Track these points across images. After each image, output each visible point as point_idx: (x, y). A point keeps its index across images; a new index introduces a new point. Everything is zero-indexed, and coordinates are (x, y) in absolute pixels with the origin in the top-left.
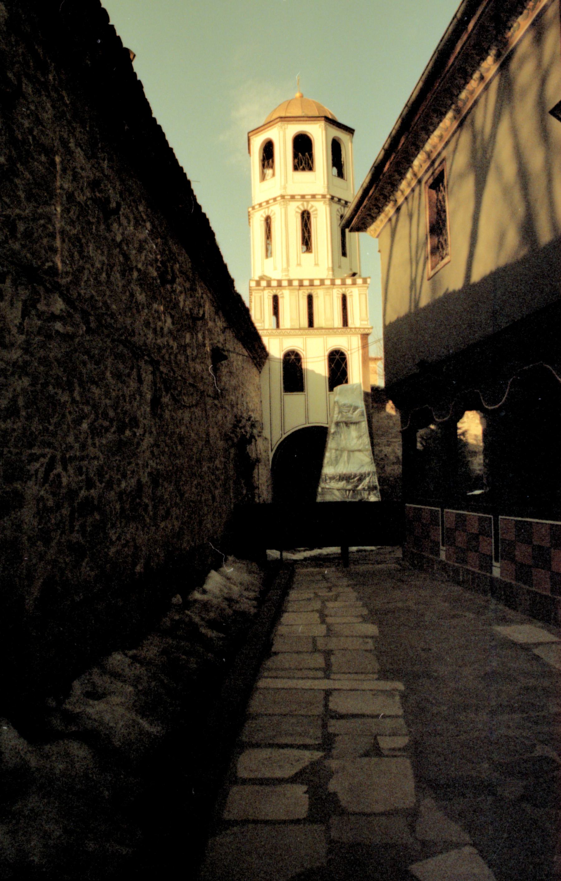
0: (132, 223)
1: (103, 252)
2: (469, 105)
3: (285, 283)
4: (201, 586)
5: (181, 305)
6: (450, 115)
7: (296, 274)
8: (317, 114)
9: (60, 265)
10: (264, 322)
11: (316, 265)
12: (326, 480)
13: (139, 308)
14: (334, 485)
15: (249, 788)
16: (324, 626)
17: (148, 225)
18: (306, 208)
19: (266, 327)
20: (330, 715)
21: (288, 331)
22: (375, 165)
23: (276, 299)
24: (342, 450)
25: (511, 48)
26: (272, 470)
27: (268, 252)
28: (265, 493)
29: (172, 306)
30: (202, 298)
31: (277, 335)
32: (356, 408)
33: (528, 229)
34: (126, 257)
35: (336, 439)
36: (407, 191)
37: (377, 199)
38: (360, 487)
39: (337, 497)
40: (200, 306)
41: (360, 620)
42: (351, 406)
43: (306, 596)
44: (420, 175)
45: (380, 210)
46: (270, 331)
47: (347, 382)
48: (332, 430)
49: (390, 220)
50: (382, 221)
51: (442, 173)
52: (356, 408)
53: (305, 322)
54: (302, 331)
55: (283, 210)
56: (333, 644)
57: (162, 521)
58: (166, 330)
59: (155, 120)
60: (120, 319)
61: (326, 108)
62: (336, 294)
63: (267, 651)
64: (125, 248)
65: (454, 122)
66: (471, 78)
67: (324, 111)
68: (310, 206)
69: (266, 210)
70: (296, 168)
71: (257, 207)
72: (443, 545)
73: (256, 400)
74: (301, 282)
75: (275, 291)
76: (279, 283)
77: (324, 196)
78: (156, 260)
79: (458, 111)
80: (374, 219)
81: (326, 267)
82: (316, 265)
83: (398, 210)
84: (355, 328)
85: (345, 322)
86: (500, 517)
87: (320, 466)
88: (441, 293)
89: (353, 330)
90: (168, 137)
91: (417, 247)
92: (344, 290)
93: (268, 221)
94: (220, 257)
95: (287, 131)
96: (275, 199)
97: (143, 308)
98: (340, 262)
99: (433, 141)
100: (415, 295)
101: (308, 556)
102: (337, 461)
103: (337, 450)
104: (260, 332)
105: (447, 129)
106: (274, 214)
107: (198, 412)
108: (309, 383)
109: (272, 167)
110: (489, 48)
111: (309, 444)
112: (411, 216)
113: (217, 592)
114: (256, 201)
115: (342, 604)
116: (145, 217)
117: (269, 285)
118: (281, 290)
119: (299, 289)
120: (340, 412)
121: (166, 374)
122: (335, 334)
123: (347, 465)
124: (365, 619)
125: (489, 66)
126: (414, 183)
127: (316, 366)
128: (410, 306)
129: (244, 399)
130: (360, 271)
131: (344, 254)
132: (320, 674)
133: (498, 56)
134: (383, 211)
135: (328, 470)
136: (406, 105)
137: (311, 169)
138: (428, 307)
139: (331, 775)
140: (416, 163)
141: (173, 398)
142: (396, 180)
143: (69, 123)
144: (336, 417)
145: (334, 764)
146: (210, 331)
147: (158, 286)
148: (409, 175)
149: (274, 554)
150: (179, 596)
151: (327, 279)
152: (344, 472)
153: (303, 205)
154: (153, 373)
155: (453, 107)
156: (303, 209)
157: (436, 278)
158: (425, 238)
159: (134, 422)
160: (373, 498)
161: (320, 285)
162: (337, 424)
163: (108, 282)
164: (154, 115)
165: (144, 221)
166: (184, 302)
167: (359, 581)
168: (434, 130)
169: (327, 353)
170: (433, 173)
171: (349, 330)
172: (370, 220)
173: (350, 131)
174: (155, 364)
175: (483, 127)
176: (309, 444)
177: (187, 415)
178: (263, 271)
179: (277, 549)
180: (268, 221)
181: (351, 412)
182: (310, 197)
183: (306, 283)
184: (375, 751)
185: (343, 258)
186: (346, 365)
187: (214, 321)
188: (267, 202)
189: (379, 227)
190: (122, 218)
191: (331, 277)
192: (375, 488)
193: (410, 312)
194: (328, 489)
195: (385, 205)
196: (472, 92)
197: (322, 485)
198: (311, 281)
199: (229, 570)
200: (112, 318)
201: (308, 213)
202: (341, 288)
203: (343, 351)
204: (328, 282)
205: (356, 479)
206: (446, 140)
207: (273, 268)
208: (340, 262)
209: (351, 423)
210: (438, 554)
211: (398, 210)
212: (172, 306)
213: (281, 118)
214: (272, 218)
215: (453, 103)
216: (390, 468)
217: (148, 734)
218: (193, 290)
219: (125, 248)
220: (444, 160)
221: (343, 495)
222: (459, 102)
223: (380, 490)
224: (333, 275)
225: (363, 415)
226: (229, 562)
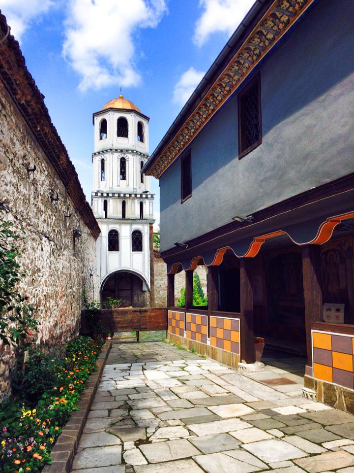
1: (26, 189)
7: (116, 189)
17: (46, 173)
30: (69, 205)
60: (33, 220)
68: (125, 156)
86: (312, 331)
109: (106, 133)
116: (45, 169)
131: (142, 181)
143: (14, 130)
173: (147, 118)
178: (99, 187)
183: (122, 195)
200: (29, 220)
210: (183, 336)
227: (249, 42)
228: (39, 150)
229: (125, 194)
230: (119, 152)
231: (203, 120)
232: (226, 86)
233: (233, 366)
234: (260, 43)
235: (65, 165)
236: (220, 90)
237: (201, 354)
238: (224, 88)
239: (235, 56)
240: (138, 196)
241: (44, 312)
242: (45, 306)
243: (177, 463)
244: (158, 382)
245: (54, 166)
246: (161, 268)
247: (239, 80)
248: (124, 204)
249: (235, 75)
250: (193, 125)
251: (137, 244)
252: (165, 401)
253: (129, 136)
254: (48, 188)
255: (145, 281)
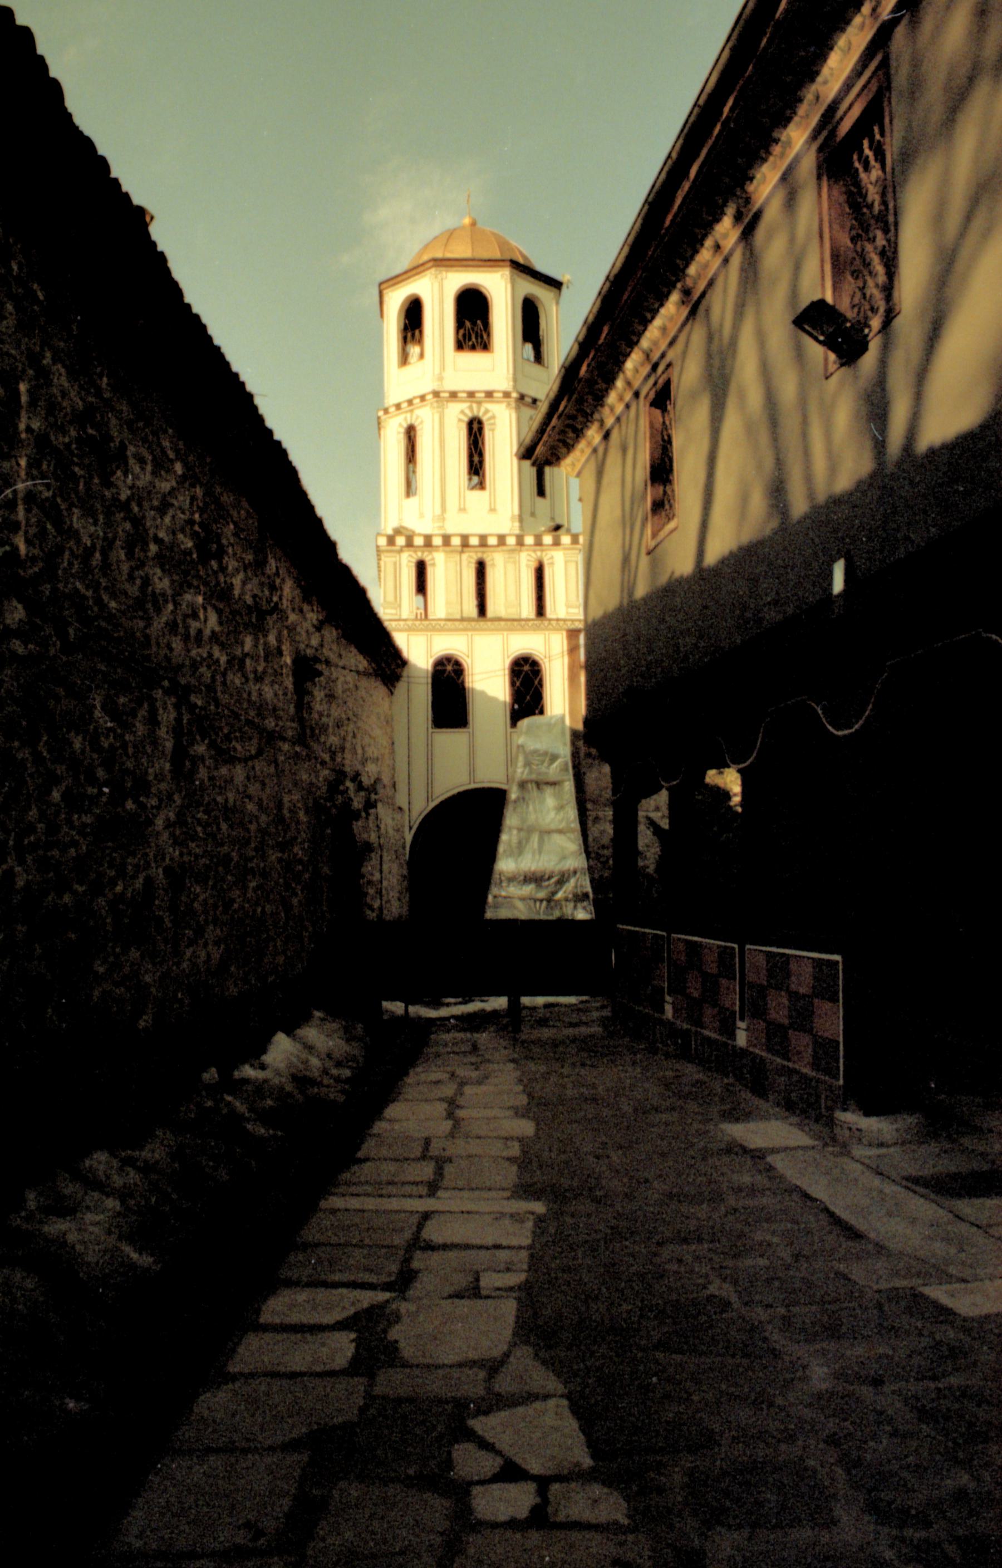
0: (149, 468)
2: (701, 286)
3: (437, 541)
4: (258, 1057)
5: (237, 592)
6: (675, 297)
7: (456, 525)
8: (498, 255)
9: (22, 548)
10: (400, 606)
11: (493, 510)
12: (501, 881)
13: (158, 601)
14: (514, 890)
15: (268, 1336)
16: (450, 1123)
17: (178, 468)
18: (476, 413)
19: (404, 616)
20: (418, 1244)
21: (442, 623)
22: (567, 364)
23: (421, 568)
24: (530, 830)
25: (755, 210)
26: (410, 864)
27: (410, 488)
28: (395, 903)
29: (220, 596)
30: (277, 574)
31: (421, 630)
32: (554, 758)
33: (778, 492)
34: (137, 522)
35: (519, 810)
36: (620, 408)
37: (573, 417)
38: (560, 895)
39: (521, 911)
40: (273, 588)
41: (511, 1113)
42: (546, 753)
43: (433, 1077)
44: (636, 384)
45: (579, 434)
46: (410, 623)
47: (542, 712)
48: (513, 795)
49: (595, 451)
50: (582, 451)
51: (668, 383)
52: (554, 758)
53: (471, 607)
54: (465, 623)
55: (437, 417)
56: (458, 1148)
57: (187, 947)
58: (207, 632)
59: (188, 306)
61: (514, 243)
62: (526, 563)
63: (349, 1158)
64: (136, 509)
65: (683, 307)
66: (702, 245)
67: (511, 249)
68: (482, 410)
69: (408, 415)
70: (460, 346)
71: (392, 409)
72: (669, 994)
73: (384, 742)
74: (465, 539)
75: (419, 554)
76: (428, 540)
77: (507, 395)
78: (191, 522)
79: (687, 292)
80: (569, 447)
81: (510, 514)
82: (493, 510)
83: (607, 436)
84: (558, 620)
85: (540, 610)
86: (748, 946)
87: (490, 856)
88: (663, 580)
89: (554, 623)
90: (211, 331)
91: (632, 503)
92: (539, 553)
93: (411, 434)
94: (310, 508)
95: (446, 282)
96: (423, 398)
97: (166, 601)
98: (533, 505)
99: (653, 335)
100: (629, 576)
101: (459, 1013)
102: (520, 849)
103: (520, 830)
104: (389, 625)
105: (671, 319)
106: (422, 422)
107: (260, 766)
108: (477, 712)
109: (420, 341)
110: (725, 205)
111: (473, 819)
112: (624, 450)
113: (282, 1066)
114: (390, 400)
115: (492, 1088)
117: (410, 544)
118: (430, 552)
119: (462, 552)
120: (527, 764)
121: (201, 708)
122: (523, 629)
123: (537, 857)
124: (520, 1113)
125: (726, 230)
126: (628, 396)
127: (489, 682)
128: (622, 598)
129: (358, 740)
130: (569, 522)
131: (541, 492)
132: (423, 1190)
133: (738, 217)
134: (584, 436)
135: (505, 865)
136: (607, 278)
138: (645, 600)
139: (397, 1318)
140: (629, 365)
141: (212, 745)
142: (601, 390)
144: (521, 772)
145: (404, 1307)
146: (292, 629)
147: (196, 564)
148: (619, 383)
149: (396, 1007)
150: (213, 1070)
151: (510, 535)
152: (533, 868)
153: (471, 408)
154: (177, 707)
155: (679, 285)
156: (470, 415)
157: (657, 550)
158: (643, 484)
159: (142, 786)
160: (582, 914)
161: (498, 546)
162: (522, 785)
163: (106, 566)
164: (187, 299)
165: (172, 461)
166: (242, 586)
167: (525, 1051)
168: (653, 318)
169: (508, 662)
170: (655, 384)
171: (546, 623)
172: (564, 450)
173: (556, 285)
174: (181, 694)
175: (721, 325)
176: (473, 819)
177: (239, 773)
178: (400, 520)
179: (401, 1001)
180: (411, 434)
181: (546, 764)
182: (483, 395)
183: (474, 541)
184: (474, 1291)
185: (539, 500)
187: (301, 611)
188: (410, 402)
189: (579, 460)
190: (131, 461)
191: (517, 531)
192: (586, 896)
193: (621, 605)
194: (505, 897)
195: (585, 426)
196: (706, 266)
197: (494, 890)
198: (483, 539)
199: (311, 1033)
201: (480, 422)
202: (535, 551)
203: (537, 658)
204: (511, 541)
205: (553, 880)
206: (672, 334)
207: (418, 515)
208: (533, 505)
209: (547, 783)
211: (607, 436)
212: (220, 596)
213: (435, 260)
214: (418, 428)
215: (679, 280)
217: (133, 1266)
218: (259, 564)
219: (136, 509)
220: (669, 365)
221: (530, 908)
222: (687, 279)
223: (594, 900)
224: (521, 528)
225: (567, 770)
226: (315, 1021)
243: (497, 1493)
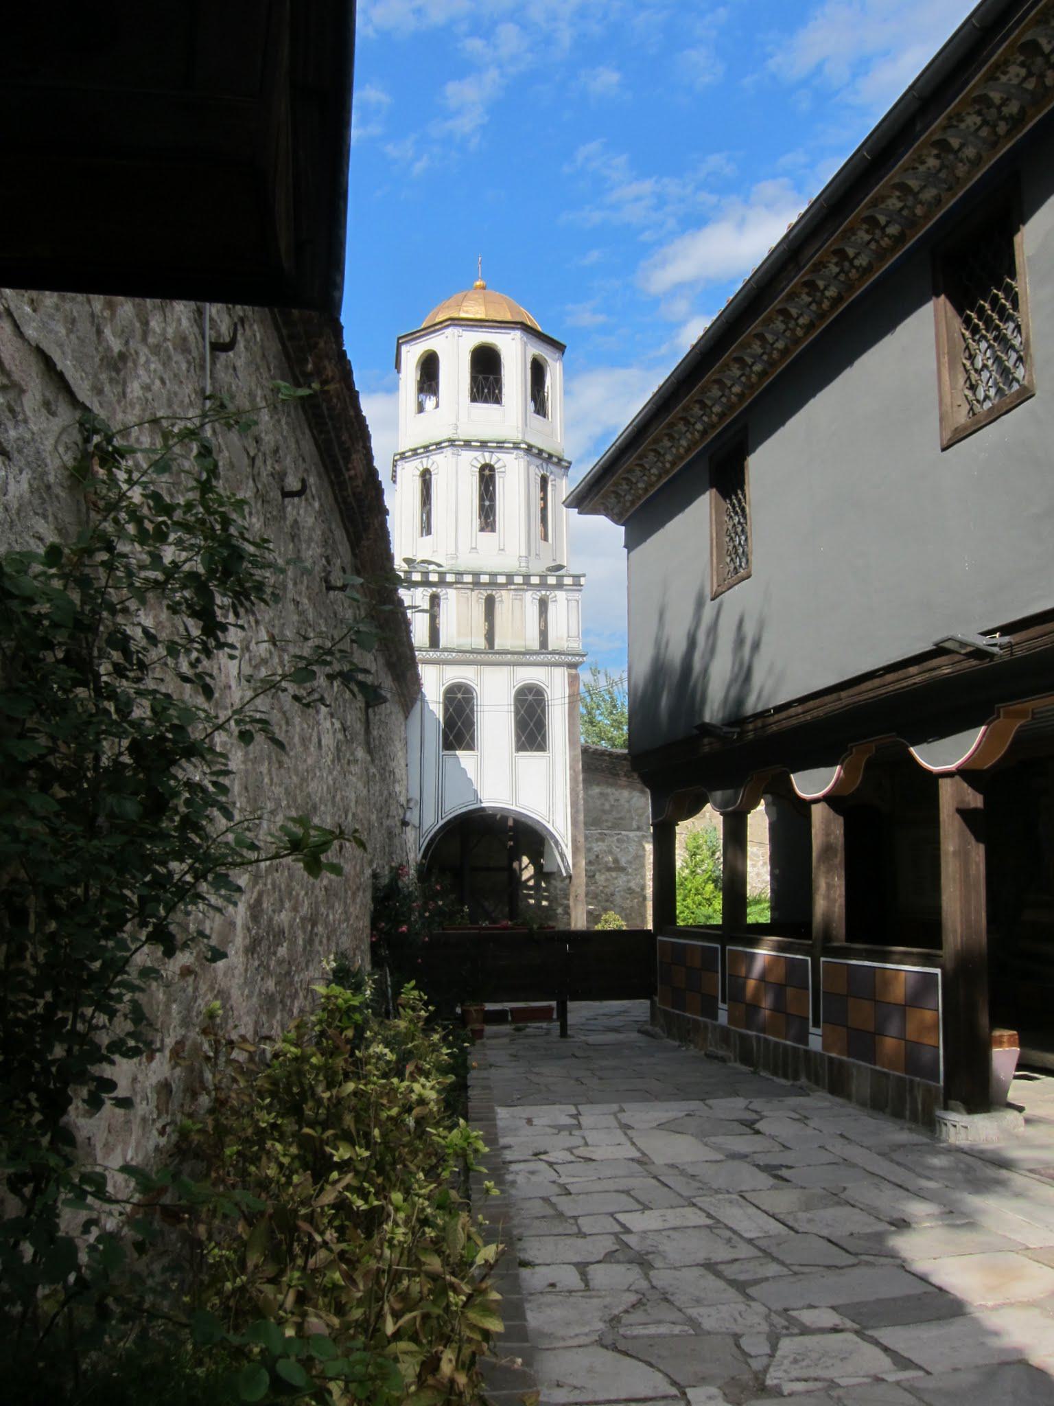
7: (467, 561)
17: (317, 505)
70: (474, 399)
72: (724, 1001)
93: (487, 515)
137: (497, 400)
180: (487, 515)
186: (543, 711)
210: (715, 1017)
216: (603, 877)
227: (991, 78)
228: (304, 434)
229: (493, 575)
230: (476, 448)
231: (799, 332)
232: (888, 223)
233: (914, 1118)
234: (1025, 79)
235: (360, 482)
236: (867, 237)
237: (785, 1076)
238: (883, 229)
239: (936, 124)
240: (535, 580)
241: (325, 941)
242: (326, 925)
244: (691, 1171)
245: (331, 483)
246: (598, 803)
247: (938, 201)
248: (490, 603)
249: (925, 186)
250: (760, 351)
251: (530, 730)
252: (750, 1241)
253: (505, 398)
254: (319, 551)
255: (557, 843)
